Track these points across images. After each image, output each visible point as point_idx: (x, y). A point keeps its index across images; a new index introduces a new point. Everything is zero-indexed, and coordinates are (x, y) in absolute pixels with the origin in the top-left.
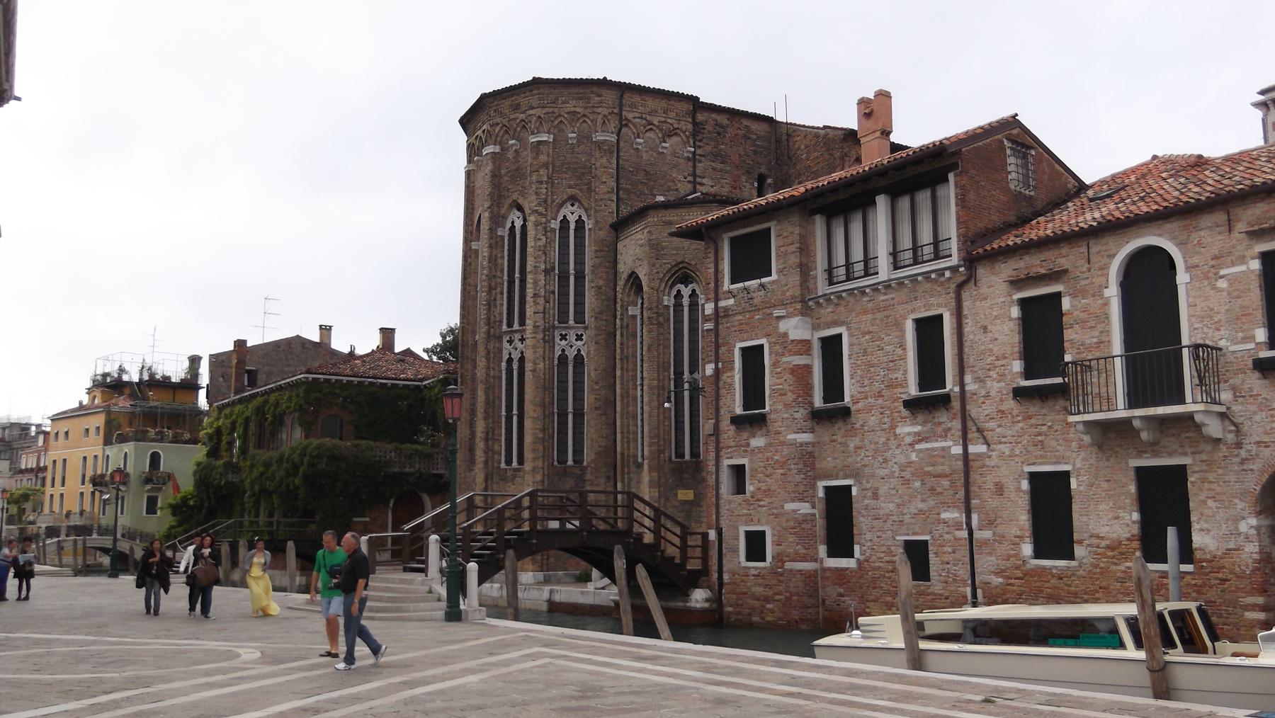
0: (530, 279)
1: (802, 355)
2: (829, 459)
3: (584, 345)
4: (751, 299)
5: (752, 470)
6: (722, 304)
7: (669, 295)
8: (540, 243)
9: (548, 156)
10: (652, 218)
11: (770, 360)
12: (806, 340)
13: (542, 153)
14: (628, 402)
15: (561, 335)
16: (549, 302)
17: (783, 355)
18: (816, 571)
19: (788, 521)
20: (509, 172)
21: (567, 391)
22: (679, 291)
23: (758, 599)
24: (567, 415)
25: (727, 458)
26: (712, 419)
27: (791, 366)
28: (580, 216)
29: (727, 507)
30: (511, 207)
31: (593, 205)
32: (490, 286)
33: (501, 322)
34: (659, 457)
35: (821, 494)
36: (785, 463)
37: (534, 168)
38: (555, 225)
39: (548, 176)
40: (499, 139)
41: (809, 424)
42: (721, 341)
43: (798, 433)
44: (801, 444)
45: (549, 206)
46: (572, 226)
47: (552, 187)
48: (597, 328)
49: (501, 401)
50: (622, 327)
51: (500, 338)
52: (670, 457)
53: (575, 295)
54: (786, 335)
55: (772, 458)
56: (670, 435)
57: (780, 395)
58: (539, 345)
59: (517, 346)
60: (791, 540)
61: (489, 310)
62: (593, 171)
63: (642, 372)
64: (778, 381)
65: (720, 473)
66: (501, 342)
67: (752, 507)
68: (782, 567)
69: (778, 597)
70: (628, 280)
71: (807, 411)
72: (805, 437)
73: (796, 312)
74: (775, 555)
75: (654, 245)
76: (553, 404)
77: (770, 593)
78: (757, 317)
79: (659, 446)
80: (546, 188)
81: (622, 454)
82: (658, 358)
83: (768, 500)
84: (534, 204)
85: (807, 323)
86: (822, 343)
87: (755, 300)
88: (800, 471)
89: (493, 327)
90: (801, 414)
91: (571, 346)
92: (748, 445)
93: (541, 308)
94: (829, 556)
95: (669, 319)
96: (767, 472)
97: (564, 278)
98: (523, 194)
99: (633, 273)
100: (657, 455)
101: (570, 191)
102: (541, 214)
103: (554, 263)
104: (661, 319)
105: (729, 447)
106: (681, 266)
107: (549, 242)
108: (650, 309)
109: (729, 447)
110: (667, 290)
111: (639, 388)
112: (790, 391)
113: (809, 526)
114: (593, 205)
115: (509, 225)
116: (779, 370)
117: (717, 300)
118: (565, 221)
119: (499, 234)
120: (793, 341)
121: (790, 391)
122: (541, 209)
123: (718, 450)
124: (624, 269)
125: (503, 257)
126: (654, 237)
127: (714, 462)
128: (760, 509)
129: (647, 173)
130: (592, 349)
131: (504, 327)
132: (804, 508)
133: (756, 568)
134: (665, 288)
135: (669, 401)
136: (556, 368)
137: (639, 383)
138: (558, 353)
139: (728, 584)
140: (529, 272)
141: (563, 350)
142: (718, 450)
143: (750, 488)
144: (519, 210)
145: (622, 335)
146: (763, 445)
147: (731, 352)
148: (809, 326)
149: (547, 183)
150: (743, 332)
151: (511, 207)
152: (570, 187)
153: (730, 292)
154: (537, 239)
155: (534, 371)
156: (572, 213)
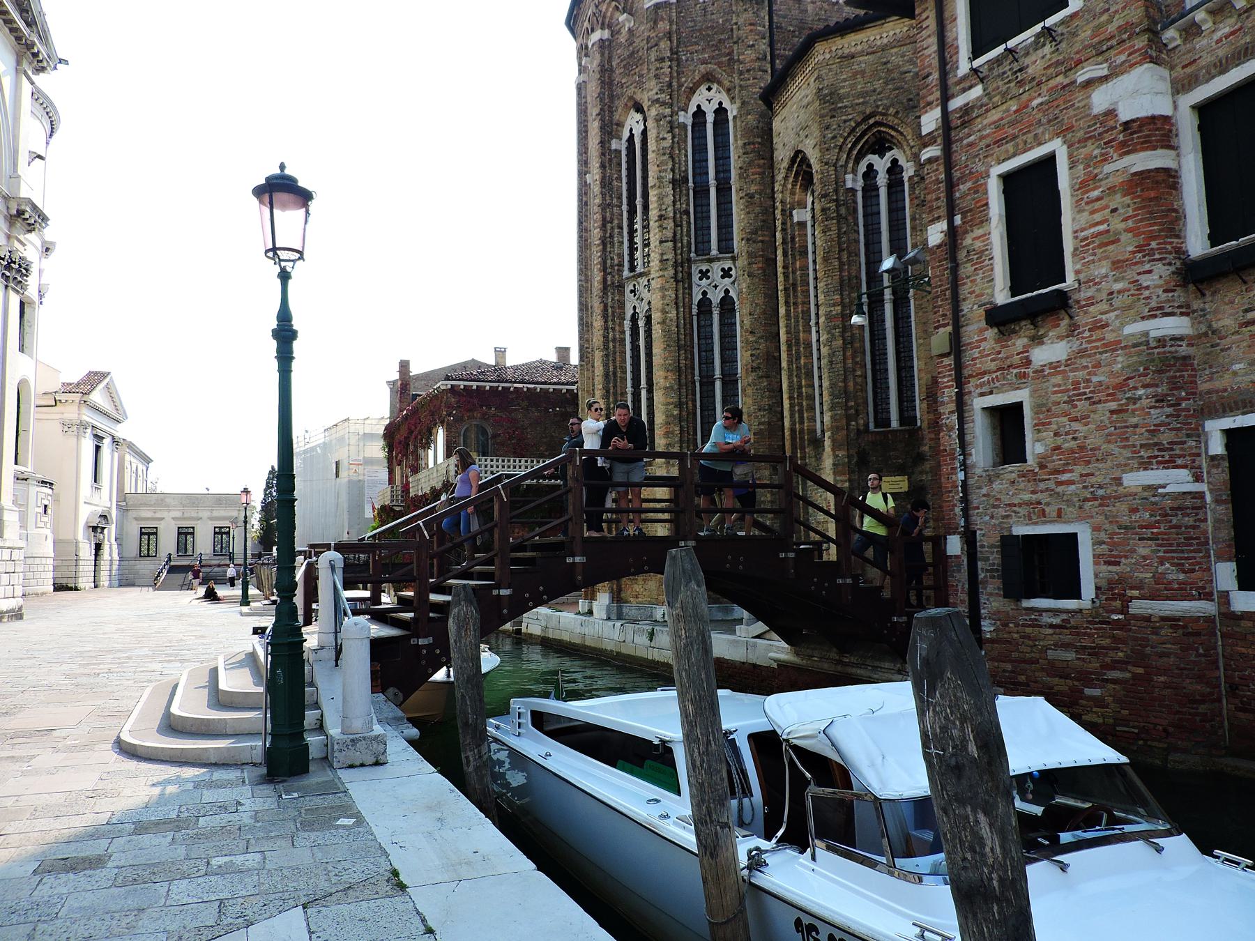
0: (653, 193)
1: (1155, 148)
2: (1237, 367)
3: (733, 283)
4: (1020, 70)
6: (956, 103)
7: (854, 172)
9: (671, 22)
10: (822, 52)
11: (1072, 178)
12: (1153, 119)
13: (662, 19)
14: (798, 352)
15: (701, 271)
16: (681, 226)
17: (1105, 159)
18: (1209, 620)
19: (1134, 510)
20: (622, 61)
21: (712, 350)
22: (870, 166)
23: (1065, 676)
24: (713, 384)
25: (982, 394)
26: (944, 325)
28: (720, 103)
29: (984, 491)
31: (737, 81)
32: (604, 219)
33: (621, 265)
34: (848, 424)
35: (1217, 446)
36: (1121, 386)
37: (653, 42)
38: (686, 118)
39: (671, 49)
40: (607, 20)
41: (1179, 296)
43: (1155, 316)
44: (1161, 341)
45: (676, 94)
46: (710, 118)
47: (678, 65)
48: (750, 254)
49: (625, 373)
50: (784, 242)
51: (621, 287)
52: (867, 425)
53: (719, 217)
54: (1111, 113)
56: (864, 390)
57: (1100, 246)
58: (668, 286)
59: (643, 295)
60: (1143, 551)
61: (604, 250)
62: (735, 32)
63: (816, 296)
64: (1098, 217)
66: (622, 294)
67: (1042, 486)
68: (1124, 610)
70: (790, 168)
71: (1172, 269)
73: (1136, 57)
74: (1104, 584)
75: (826, 95)
76: (693, 369)
77: (1095, 665)
79: (847, 408)
80: (670, 67)
81: (793, 430)
82: (841, 270)
83: (1080, 469)
84: (654, 92)
85: (1162, 78)
86: (1200, 117)
87: (1030, 70)
88: (1160, 399)
89: (610, 273)
90: (1158, 275)
91: (716, 287)
92: (1028, 362)
93: (669, 234)
94: (1241, 588)
95: (855, 210)
96: (1075, 413)
97: (701, 192)
98: (640, 85)
99: (798, 152)
100: (844, 422)
101: (703, 68)
102: (663, 104)
103: (686, 170)
104: (843, 211)
105: (985, 373)
106: (871, 121)
107: (678, 143)
108: (825, 196)
109: (985, 373)
110: (850, 165)
111: (814, 330)
112: (1128, 230)
113: (1189, 521)
114: (737, 81)
115: (626, 135)
116: (1096, 193)
118: (699, 114)
119: (613, 147)
120: (1127, 125)
121: (1128, 230)
122: (663, 97)
123: (960, 381)
124: (782, 155)
125: (619, 179)
126: (826, 83)
127: (953, 406)
128: (1060, 489)
130: (744, 285)
131: (626, 273)
132: (1177, 481)
133: (1056, 611)
134: (847, 162)
135: (860, 312)
136: (695, 318)
137: (813, 322)
138: (697, 297)
139: (991, 641)
140: (652, 187)
141: (705, 293)
142: (960, 381)
143: (1034, 447)
144: (637, 111)
145: (785, 254)
146: (1064, 357)
147: (980, 189)
148: (1166, 87)
149: (671, 60)
150: (1001, 141)
152: (704, 62)
153: (975, 71)
154: (660, 139)
155: (663, 322)
156: (707, 99)
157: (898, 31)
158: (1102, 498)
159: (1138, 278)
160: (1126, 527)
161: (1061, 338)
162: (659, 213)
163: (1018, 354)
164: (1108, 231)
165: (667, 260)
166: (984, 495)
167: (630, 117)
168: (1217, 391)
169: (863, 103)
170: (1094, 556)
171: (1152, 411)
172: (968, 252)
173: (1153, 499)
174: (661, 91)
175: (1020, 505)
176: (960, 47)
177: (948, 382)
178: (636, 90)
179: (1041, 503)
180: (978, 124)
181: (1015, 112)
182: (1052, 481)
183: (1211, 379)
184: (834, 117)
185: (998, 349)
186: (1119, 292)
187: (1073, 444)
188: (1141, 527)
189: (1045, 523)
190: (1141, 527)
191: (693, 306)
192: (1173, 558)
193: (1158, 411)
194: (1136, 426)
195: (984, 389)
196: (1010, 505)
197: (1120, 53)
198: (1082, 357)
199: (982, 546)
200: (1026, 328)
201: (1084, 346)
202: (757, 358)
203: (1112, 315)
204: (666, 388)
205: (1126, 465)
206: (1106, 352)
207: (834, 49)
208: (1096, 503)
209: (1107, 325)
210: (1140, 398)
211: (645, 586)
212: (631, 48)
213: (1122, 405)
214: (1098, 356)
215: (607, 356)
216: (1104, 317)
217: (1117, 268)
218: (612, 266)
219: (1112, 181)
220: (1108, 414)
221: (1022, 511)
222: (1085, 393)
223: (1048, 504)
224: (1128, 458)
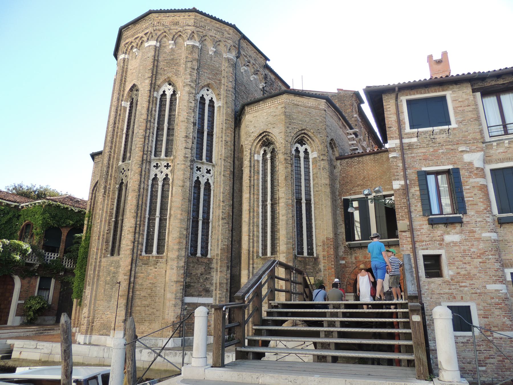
3: (211, 177)
5: (449, 258)
8: (190, 105)
22: (297, 148)
27: (479, 185)
29: (426, 287)
30: (165, 81)
42: (407, 166)
55: (470, 250)
65: (418, 261)
66: (150, 165)
69: (491, 361)
72: (494, 236)
78: (441, 151)
92: (443, 240)
101: (209, 81)
105: (423, 241)
106: (303, 132)
117: (401, 138)
118: (164, 94)
122: (192, 84)
123: (414, 243)
129: (246, 88)
138: (152, 176)
141: (198, 178)
143: (447, 271)
144: (170, 84)
146: (459, 240)
151: (165, 81)
152: (209, 78)
157: (314, 104)
158: (479, 293)
159: (486, 218)
160: (490, 304)
161: (457, 233)
162: (185, 135)
163: (438, 236)
164: (473, 201)
165: (187, 157)
166: (426, 289)
167: (164, 85)
168: (508, 260)
169: (301, 124)
170: (478, 315)
171: (495, 264)
172: (413, 195)
173: (498, 295)
174: (192, 81)
175: (444, 294)
176: (406, 122)
177: (405, 242)
178: (173, 75)
179: (453, 294)
180: (415, 151)
181: (432, 152)
182: (458, 286)
183: (505, 255)
184: (290, 124)
185: (429, 233)
186: (479, 221)
187: (465, 272)
188: (495, 304)
189: (456, 301)
190: (495, 304)
191: (149, 181)
192: (507, 316)
193: (497, 264)
194: (490, 268)
195: (424, 247)
196: (439, 294)
197: (473, 146)
198: (466, 241)
199: (428, 310)
200: (442, 227)
201: (467, 238)
202: (225, 214)
203: (477, 229)
204: (181, 220)
205: (487, 282)
206: (476, 241)
207: (291, 99)
208: (477, 295)
209: (475, 232)
210: (490, 259)
211: (150, 327)
212: (172, 57)
213: (484, 260)
214: (473, 242)
215: (139, 195)
216: (474, 229)
217: (478, 213)
218: (147, 151)
219: (474, 185)
220: (479, 263)
221: (446, 296)
222: (469, 254)
223: (456, 294)
224: (488, 279)
